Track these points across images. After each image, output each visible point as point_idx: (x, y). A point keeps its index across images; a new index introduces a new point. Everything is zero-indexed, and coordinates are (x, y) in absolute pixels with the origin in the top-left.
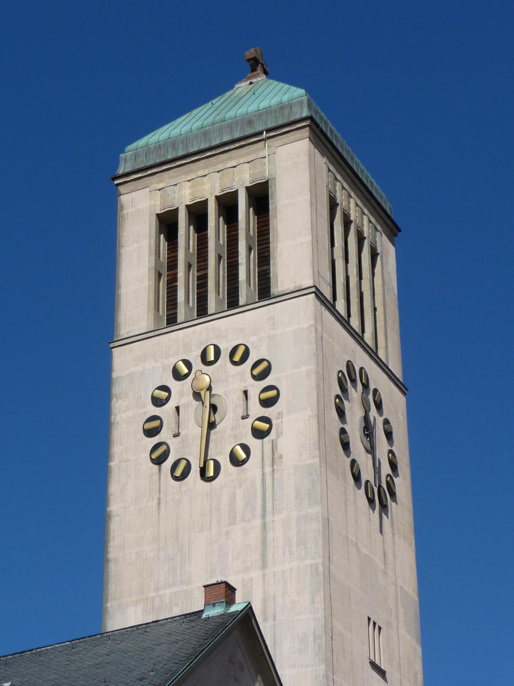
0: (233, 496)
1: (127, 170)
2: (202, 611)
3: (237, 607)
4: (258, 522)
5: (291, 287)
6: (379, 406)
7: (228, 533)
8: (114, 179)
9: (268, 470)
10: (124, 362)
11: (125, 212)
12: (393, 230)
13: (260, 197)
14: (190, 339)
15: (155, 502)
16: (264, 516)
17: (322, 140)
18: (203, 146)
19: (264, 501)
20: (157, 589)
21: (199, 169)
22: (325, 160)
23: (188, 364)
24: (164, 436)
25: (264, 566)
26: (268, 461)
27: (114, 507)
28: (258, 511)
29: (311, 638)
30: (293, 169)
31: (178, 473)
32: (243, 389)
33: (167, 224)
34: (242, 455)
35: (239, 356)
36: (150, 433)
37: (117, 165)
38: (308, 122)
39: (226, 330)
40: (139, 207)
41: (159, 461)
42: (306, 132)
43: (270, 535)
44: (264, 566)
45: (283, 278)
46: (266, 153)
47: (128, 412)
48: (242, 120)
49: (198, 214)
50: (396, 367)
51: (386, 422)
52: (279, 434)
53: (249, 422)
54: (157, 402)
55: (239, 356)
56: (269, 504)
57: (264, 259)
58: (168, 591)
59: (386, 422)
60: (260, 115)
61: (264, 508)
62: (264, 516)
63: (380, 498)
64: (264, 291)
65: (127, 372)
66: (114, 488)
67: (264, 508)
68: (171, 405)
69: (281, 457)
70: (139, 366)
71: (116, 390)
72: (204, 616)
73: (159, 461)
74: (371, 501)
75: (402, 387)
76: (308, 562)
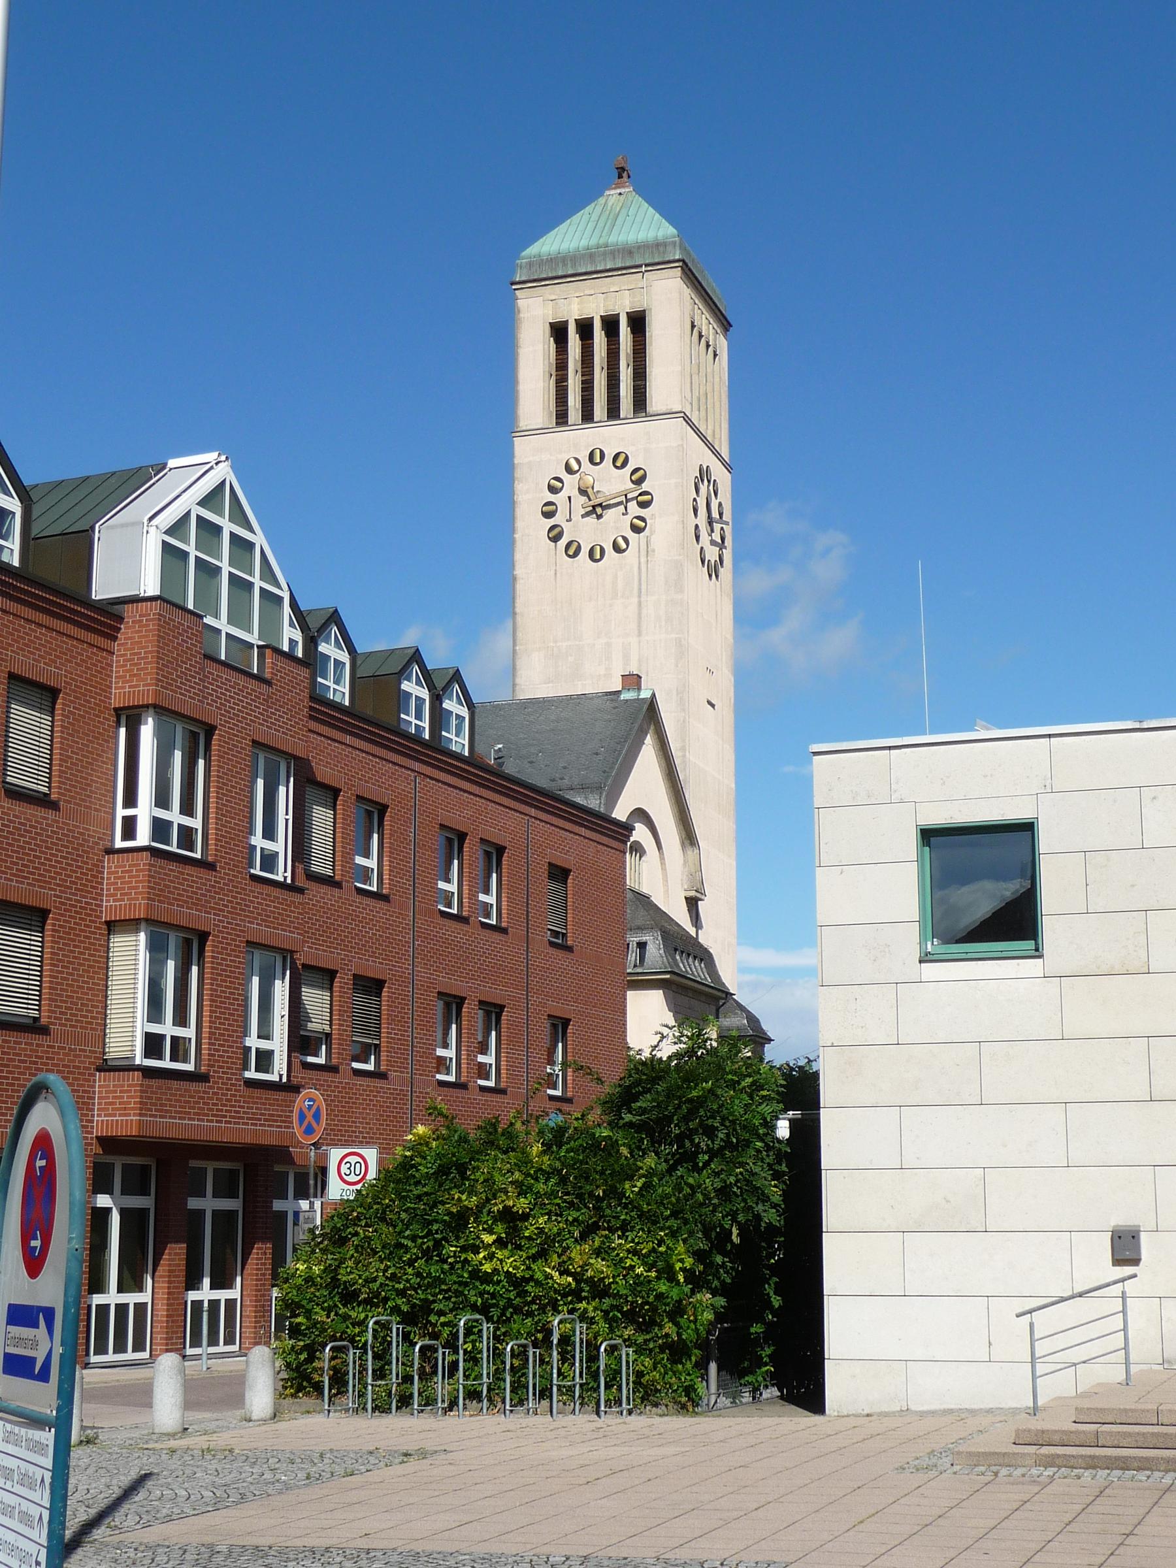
0: (616, 577)
1: (524, 278)
2: (619, 692)
3: (645, 694)
4: (635, 600)
5: (663, 409)
6: (716, 494)
7: (611, 605)
8: (512, 284)
9: (643, 560)
10: (524, 449)
11: (522, 315)
12: (725, 324)
13: (638, 322)
14: (579, 439)
15: (553, 572)
16: (639, 596)
17: (691, 277)
18: (589, 269)
19: (640, 584)
20: (556, 642)
21: (588, 286)
22: (689, 291)
23: (578, 461)
24: (558, 519)
25: (640, 634)
26: (643, 553)
27: (519, 571)
28: (636, 591)
29: (675, 692)
30: (667, 300)
31: (571, 552)
32: (1121, 1219)
33: (559, 332)
34: (624, 546)
35: (621, 461)
36: (548, 515)
37: (513, 269)
38: (680, 264)
39: (609, 436)
40: (535, 311)
41: (555, 539)
42: (678, 272)
43: (644, 611)
44: (640, 634)
45: (657, 399)
46: (644, 283)
47: (529, 496)
48: (624, 249)
49: (585, 328)
50: (725, 454)
51: (720, 504)
52: (652, 533)
53: (629, 518)
54: (553, 490)
55: (621, 461)
56: (644, 587)
57: (640, 374)
58: (564, 644)
59: (720, 504)
60: (639, 247)
61: (640, 590)
62: (639, 596)
63: (714, 571)
64: (640, 402)
65: (526, 460)
66: (518, 556)
67: (640, 590)
68: (563, 494)
69: (653, 551)
70: (542, 453)
71: (518, 474)
72: (622, 697)
73: (555, 539)
74: (710, 576)
75: (728, 467)
76: (674, 636)
